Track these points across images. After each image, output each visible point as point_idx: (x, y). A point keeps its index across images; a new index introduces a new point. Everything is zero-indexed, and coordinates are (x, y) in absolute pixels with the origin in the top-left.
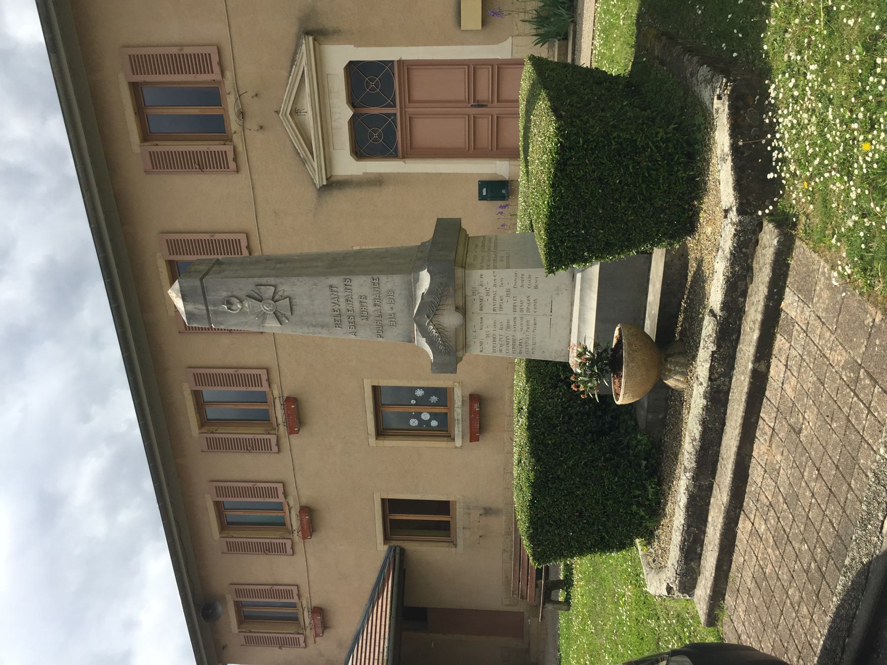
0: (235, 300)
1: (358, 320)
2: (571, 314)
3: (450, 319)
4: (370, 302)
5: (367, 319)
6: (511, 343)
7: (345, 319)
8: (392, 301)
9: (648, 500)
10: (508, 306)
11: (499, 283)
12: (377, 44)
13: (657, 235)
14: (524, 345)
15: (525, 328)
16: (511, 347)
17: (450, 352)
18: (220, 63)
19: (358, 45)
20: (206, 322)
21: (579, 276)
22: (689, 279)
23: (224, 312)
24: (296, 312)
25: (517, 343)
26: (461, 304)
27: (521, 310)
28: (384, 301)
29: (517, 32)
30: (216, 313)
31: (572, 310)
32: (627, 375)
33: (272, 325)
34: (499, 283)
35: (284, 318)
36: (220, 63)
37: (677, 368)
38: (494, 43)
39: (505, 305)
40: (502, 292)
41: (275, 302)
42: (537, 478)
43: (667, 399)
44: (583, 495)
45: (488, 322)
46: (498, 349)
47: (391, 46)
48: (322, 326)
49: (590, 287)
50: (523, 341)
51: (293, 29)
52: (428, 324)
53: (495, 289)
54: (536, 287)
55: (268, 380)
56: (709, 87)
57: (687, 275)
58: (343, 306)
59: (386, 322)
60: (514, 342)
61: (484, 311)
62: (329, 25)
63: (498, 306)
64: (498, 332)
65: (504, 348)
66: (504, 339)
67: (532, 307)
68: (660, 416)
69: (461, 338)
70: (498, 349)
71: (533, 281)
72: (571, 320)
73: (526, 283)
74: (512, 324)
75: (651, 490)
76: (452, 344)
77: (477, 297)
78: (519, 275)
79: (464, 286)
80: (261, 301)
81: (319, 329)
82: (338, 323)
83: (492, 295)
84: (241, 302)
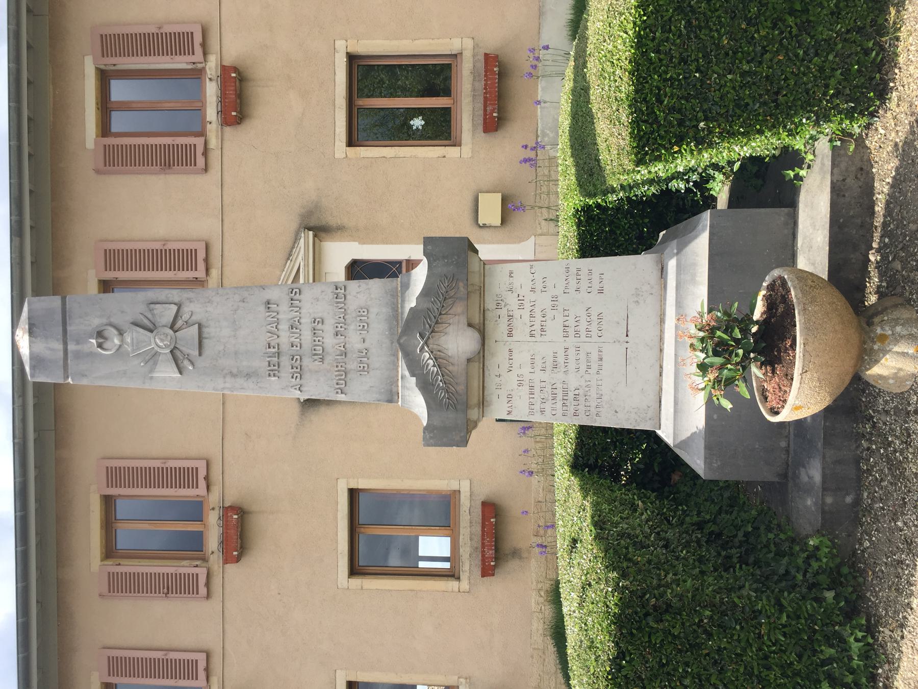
0: (111, 332)
1: (307, 362)
2: (661, 339)
3: (458, 342)
4: (328, 328)
5: (322, 360)
7: (285, 361)
8: (365, 327)
9: (852, 671)
10: (554, 328)
11: (539, 286)
12: (385, 241)
13: (825, 94)
14: (582, 398)
15: (583, 367)
16: (559, 405)
17: (456, 408)
18: (206, 260)
19: (362, 241)
20: (60, 373)
21: (672, 264)
22: (879, 208)
23: (92, 355)
24: (207, 351)
25: (571, 395)
26: (476, 320)
27: (577, 333)
28: (352, 327)
29: (539, 231)
30: (78, 355)
31: (662, 331)
32: (807, 329)
33: (166, 372)
35: (186, 362)
36: (206, 260)
37: (898, 329)
38: (515, 243)
39: (549, 324)
40: (544, 301)
41: (175, 332)
42: (623, 604)
43: (857, 461)
44: (719, 650)
45: (522, 357)
46: (537, 407)
47: (400, 243)
48: (248, 376)
49: (693, 281)
50: (581, 392)
51: (294, 226)
52: (422, 349)
53: (533, 297)
54: (601, 291)
55: (207, 670)
57: (872, 204)
58: (285, 338)
59: (352, 365)
60: (565, 394)
61: (515, 338)
62: (332, 221)
63: (537, 327)
65: (548, 406)
66: (549, 389)
67: (594, 328)
68: (849, 499)
69: (475, 384)
70: (537, 407)
71: (596, 278)
72: (661, 350)
73: (584, 285)
74: (561, 359)
75: (855, 647)
76: (461, 388)
77: (503, 312)
78: (573, 270)
79: (482, 291)
80: (151, 331)
81: (240, 381)
82: (274, 370)
83: (527, 306)
84: (121, 333)
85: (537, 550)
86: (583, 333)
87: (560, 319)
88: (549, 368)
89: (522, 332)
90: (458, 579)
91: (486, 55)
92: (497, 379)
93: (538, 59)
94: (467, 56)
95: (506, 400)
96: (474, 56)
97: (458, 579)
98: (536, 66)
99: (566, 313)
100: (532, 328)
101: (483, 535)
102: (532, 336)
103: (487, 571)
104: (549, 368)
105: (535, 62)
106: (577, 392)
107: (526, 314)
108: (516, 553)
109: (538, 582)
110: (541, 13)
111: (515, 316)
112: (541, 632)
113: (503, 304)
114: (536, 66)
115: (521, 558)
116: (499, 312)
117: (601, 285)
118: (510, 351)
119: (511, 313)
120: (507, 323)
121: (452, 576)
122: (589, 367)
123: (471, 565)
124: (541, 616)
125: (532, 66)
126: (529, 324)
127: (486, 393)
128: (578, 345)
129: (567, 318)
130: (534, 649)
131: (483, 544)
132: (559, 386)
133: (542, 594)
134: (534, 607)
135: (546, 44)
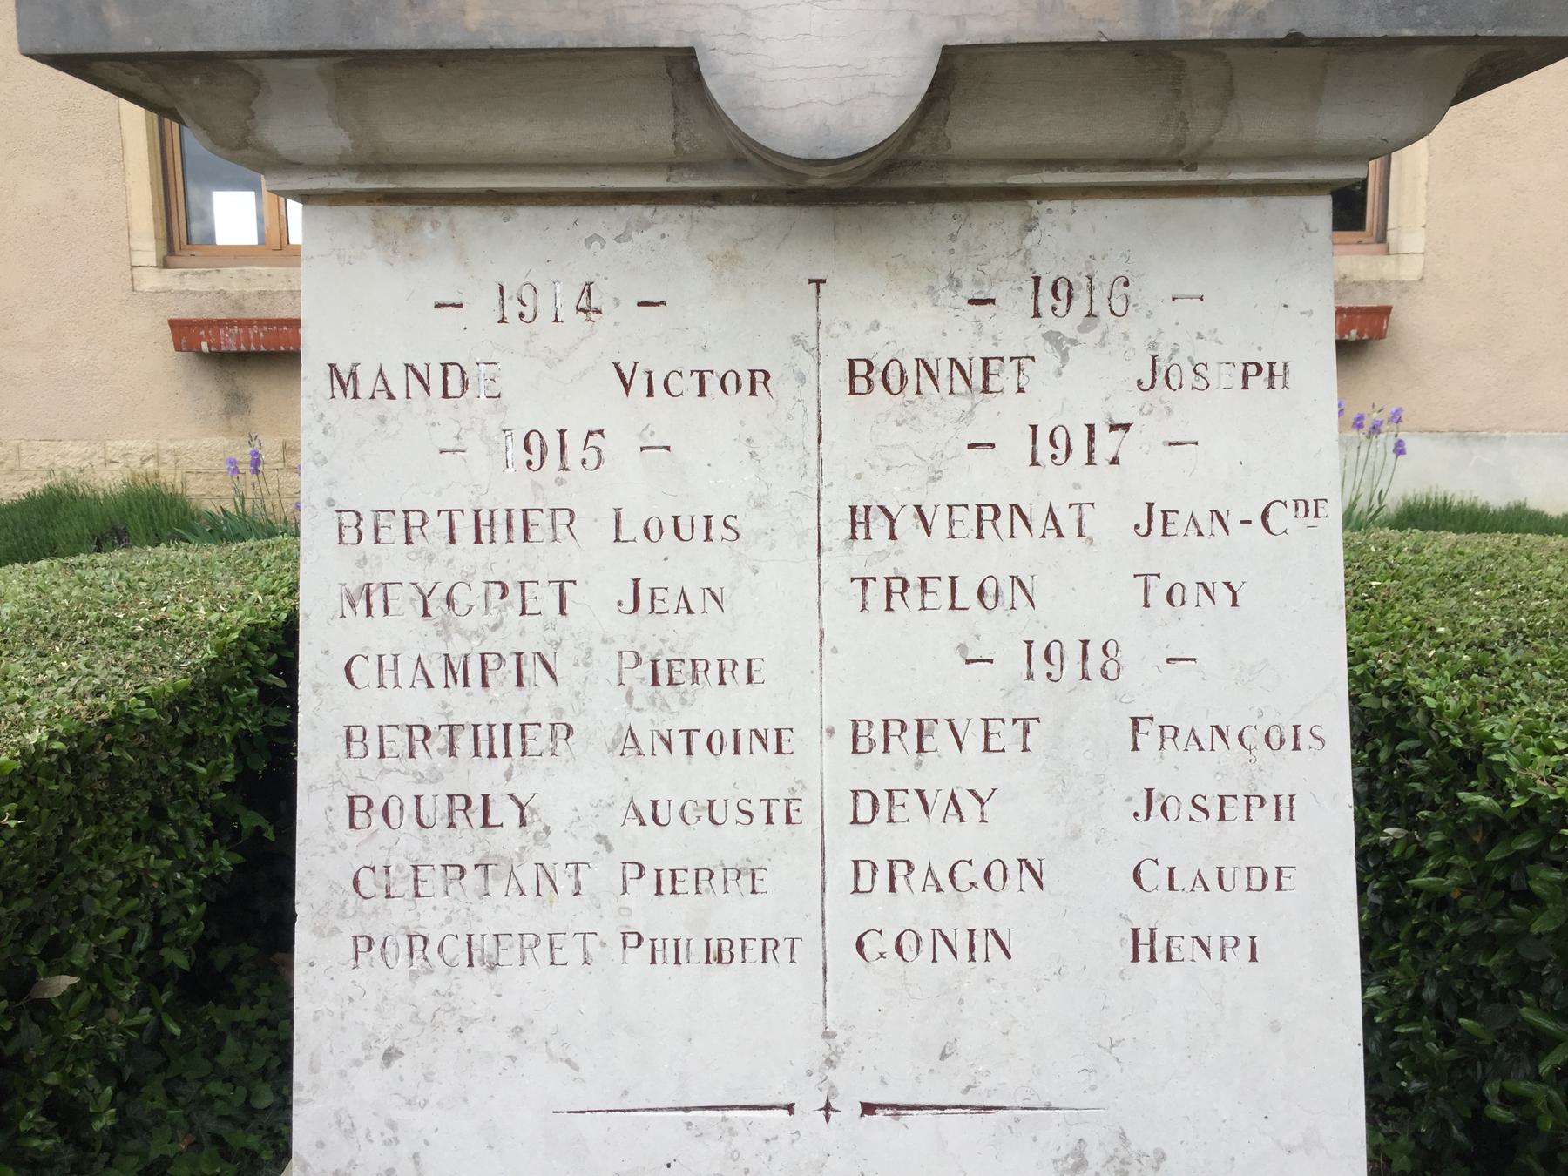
6: (470, 706)
10: (913, 666)
11: (1180, 559)
14: (465, 843)
16: (419, 706)
25: (481, 777)
27: (876, 805)
34: (1180, 559)
39: (929, 630)
40: (1083, 592)
45: (717, 459)
46: (391, 562)
50: (507, 837)
56: (248, 504)
60: (490, 742)
61: (841, 409)
63: (916, 554)
64: (601, 572)
66: (519, 634)
67: (915, 908)
73: (1187, 843)
74: (711, 708)
77: (1011, 328)
78: (1278, 773)
85: (244, 455)
86: (879, 841)
87: (967, 697)
88: (650, 633)
89: (880, 449)
90: (164, 264)
91: (1385, 311)
92: (569, 296)
93: (1375, 429)
94: (1386, 268)
95: (429, 358)
96: (1382, 283)
97: (164, 264)
98: (1360, 426)
99: (1007, 736)
100: (907, 523)
101: (270, 322)
102: (859, 519)
103: (184, 332)
104: (650, 633)
105: (1367, 424)
106: (503, 812)
107: (1003, 478)
108: (237, 403)
109: (175, 453)
110: (1463, 435)
111: (986, 407)
112: (60, 463)
113: (1067, 326)
114: (1360, 426)
115: (229, 413)
116: (1014, 301)
117: (1184, 948)
118: (758, 380)
119: (1005, 379)
120: (939, 355)
121: (171, 251)
122: (666, 883)
123: (200, 294)
124: (97, 461)
125: (1361, 418)
126: (935, 500)
127: (466, 216)
128: (807, 813)
129: (974, 742)
130: (19, 449)
131: (249, 323)
132: (541, 701)
133: (150, 465)
134: (116, 446)
135: (1408, 447)
